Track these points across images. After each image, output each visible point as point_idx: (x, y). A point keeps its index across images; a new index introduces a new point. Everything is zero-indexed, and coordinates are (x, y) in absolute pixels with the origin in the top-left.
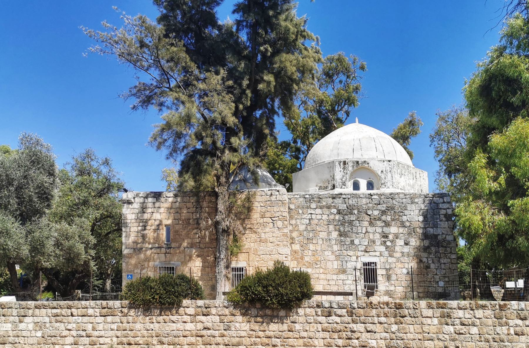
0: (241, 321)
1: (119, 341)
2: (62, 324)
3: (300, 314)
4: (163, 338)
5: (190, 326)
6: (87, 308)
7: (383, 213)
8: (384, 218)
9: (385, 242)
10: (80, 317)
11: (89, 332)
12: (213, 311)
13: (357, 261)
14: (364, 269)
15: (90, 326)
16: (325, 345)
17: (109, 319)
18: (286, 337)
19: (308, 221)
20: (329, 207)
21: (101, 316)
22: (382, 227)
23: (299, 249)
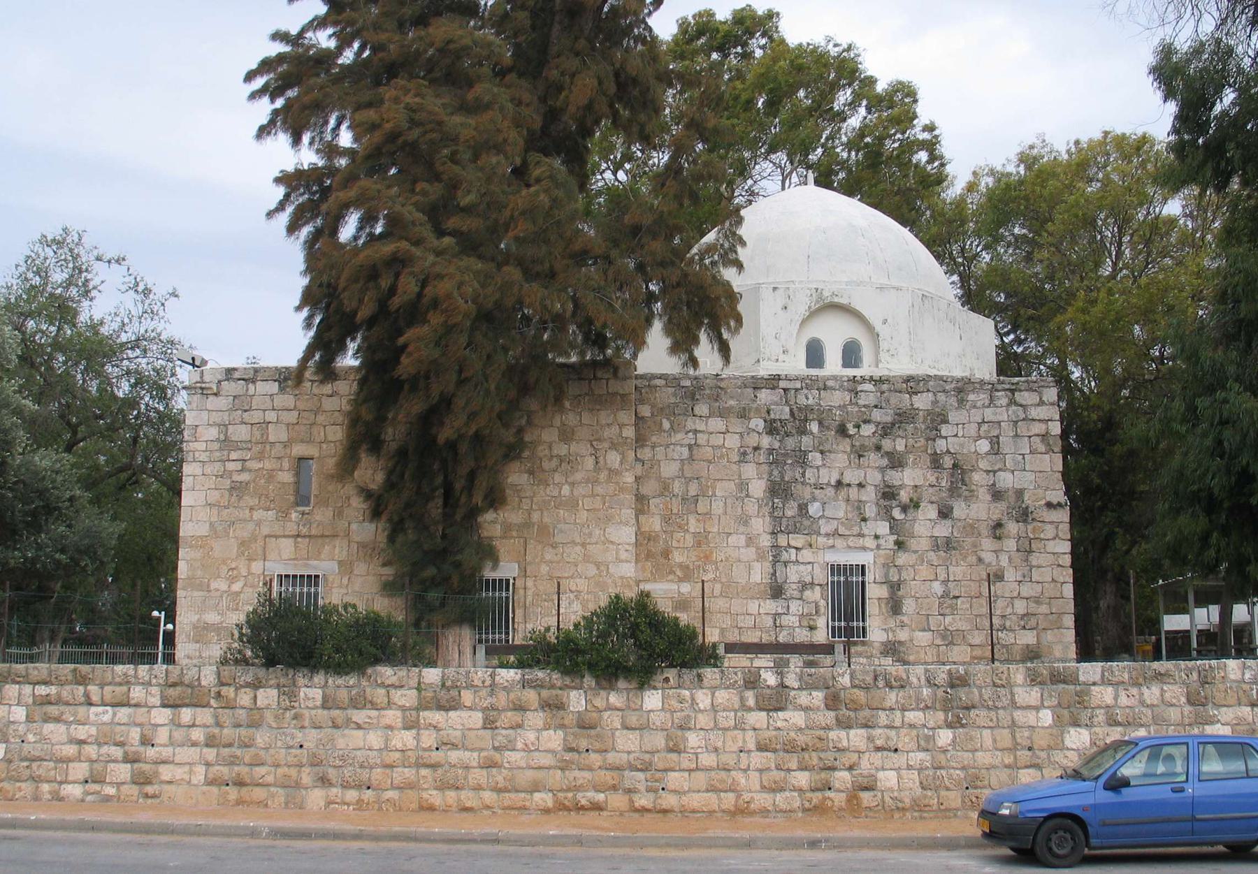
0: (541, 724)
1: (210, 776)
2: (62, 728)
3: (701, 706)
4: (330, 770)
5: (405, 738)
6: (128, 683)
7: (886, 430)
8: (887, 444)
9: (888, 510)
10: (108, 708)
11: (133, 749)
12: (467, 697)
13: (812, 562)
14: (833, 582)
15: (135, 734)
16: (763, 787)
17: (186, 714)
18: (661, 766)
19: (685, 451)
20: (743, 415)
21: (164, 706)
22: (882, 470)
23: (658, 528)
